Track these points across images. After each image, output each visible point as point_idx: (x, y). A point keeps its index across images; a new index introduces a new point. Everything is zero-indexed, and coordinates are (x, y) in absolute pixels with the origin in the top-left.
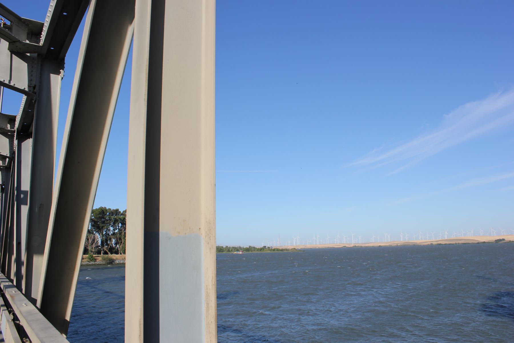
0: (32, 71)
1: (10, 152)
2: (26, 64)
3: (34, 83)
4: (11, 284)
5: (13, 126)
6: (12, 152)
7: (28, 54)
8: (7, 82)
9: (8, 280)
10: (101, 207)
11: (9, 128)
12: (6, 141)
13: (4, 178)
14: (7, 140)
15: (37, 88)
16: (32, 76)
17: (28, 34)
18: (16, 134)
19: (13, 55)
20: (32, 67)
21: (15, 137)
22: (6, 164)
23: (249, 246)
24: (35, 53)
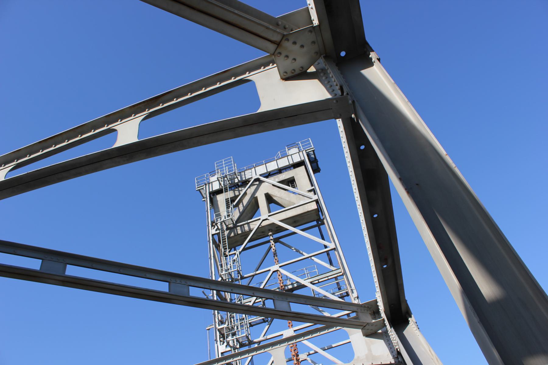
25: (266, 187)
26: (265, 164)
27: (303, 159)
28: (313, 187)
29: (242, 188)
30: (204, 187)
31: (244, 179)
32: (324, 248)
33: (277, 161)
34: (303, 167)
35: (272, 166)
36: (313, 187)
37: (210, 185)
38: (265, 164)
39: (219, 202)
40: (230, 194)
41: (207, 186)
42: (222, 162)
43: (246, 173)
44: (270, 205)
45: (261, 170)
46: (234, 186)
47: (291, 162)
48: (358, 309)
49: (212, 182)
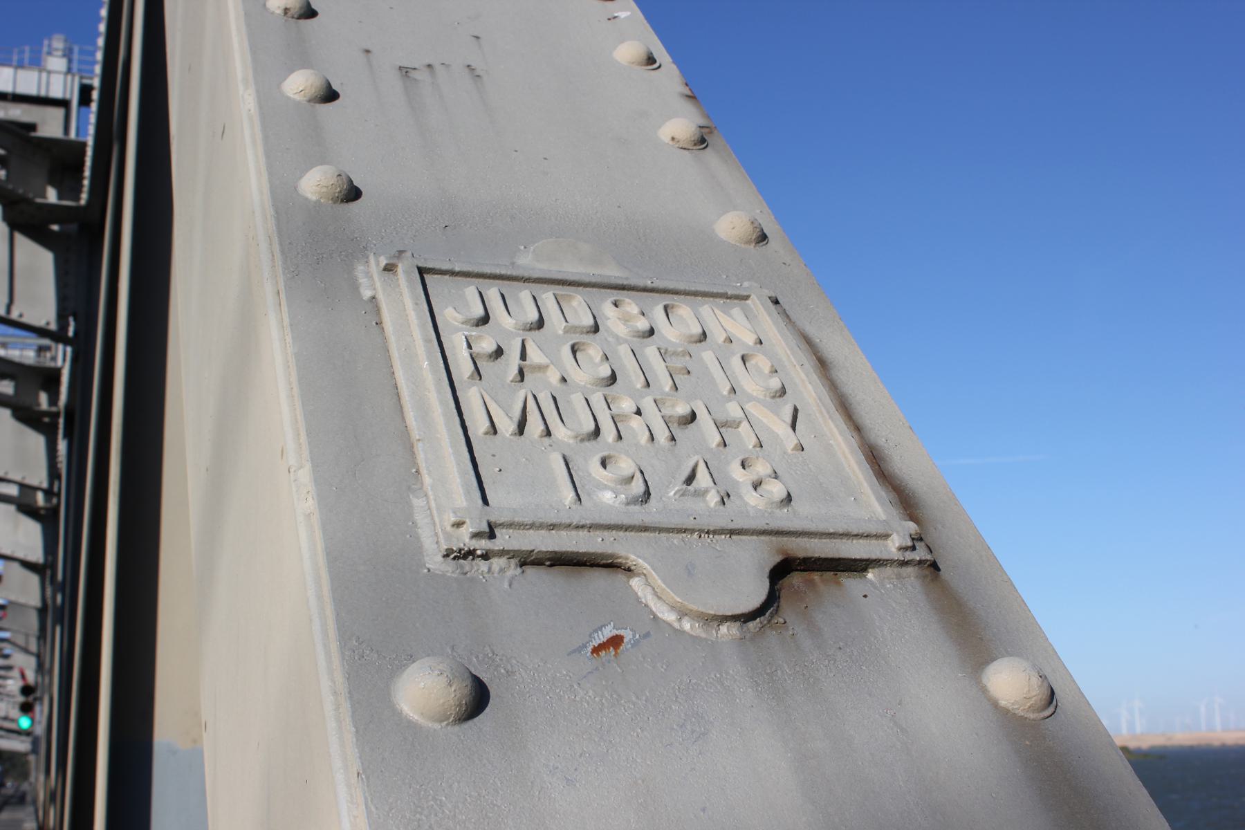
5: (54, 400)
7: (55, 227)
12: (37, 441)
22: (84, 197)
27: (68, 96)
47: (43, 93)
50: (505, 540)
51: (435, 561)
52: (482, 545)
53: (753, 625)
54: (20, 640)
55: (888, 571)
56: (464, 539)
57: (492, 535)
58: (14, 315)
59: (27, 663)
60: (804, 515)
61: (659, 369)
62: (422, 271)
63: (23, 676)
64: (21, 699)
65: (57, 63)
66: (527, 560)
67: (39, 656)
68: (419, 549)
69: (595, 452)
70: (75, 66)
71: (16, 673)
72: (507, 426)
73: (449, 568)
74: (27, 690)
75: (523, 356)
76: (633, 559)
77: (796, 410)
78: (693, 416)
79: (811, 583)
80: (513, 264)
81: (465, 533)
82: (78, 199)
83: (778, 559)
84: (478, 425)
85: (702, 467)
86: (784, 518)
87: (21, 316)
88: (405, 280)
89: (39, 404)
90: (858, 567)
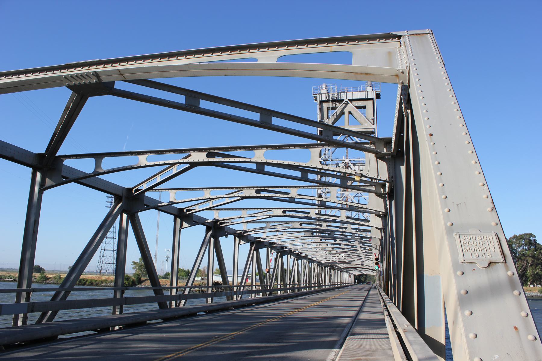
0: (389, 167)
1: (385, 209)
2: (386, 163)
3: (391, 175)
4: (391, 301)
5: (385, 191)
6: (386, 209)
7: (386, 157)
8: (376, 177)
9: (390, 300)
10: (514, 235)
11: (382, 192)
12: (381, 201)
13: (384, 222)
14: (382, 200)
15: (394, 177)
16: (390, 170)
17: (384, 144)
18: (387, 195)
19: (378, 159)
20: (389, 165)
21: (387, 199)
22: (392, 150)
23: (184, 268)
24: (389, 156)
25: (351, 107)
26: (353, 92)
27: (373, 97)
28: (374, 118)
29: (337, 103)
30: (317, 95)
31: (340, 99)
32: (386, 328)
33: (360, 92)
34: (372, 101)
35: (356, 96)
36: (374, 118)
37: (321, 95)
38: (353, 92)
39: (324, 108)
40: (330, 105)
41: (319, 95)
42: (330, 86)
43: (341, 94)
44: (349, 115)
45: (350, 96)
46: (333, 101)
47: (366, 97)
48: (332, 129)
49: (322, 94)
50: (466, 261)
51: (460, 263)
52: (463, 262)
53: (486, 268)
54: (375, 246)
55: (500, 263)
56: (462, 261)
57: (464, 261)
58: (379, 178)
59: (377, 252)
60: (494, 258)
61: (481, 244)
62: (459, 234)
63: (375, 255)
64: (376, 261)
65: (370, 89)
66: (467, 263)
67: (379, 251)
68: (459, 261)
69: (474, 253)
70: (374, 89)
71: (373, 255)
72: (466, 251)
73: (461, 263)
74: (377, 259)
75: (468, 243)
76: (476, 263)
77: (495, 247)
78: (484, 248)
79: (493, 264)
80: (468, 232)
81: (462, 260)
82: (391, 151)
83: (490, 262)
84: (464, 251)
85: (484, 254)
86: (491, 259)
87: (381, 178)
88: (458, 236)
89: (381, 192)
90: (498, 263)
